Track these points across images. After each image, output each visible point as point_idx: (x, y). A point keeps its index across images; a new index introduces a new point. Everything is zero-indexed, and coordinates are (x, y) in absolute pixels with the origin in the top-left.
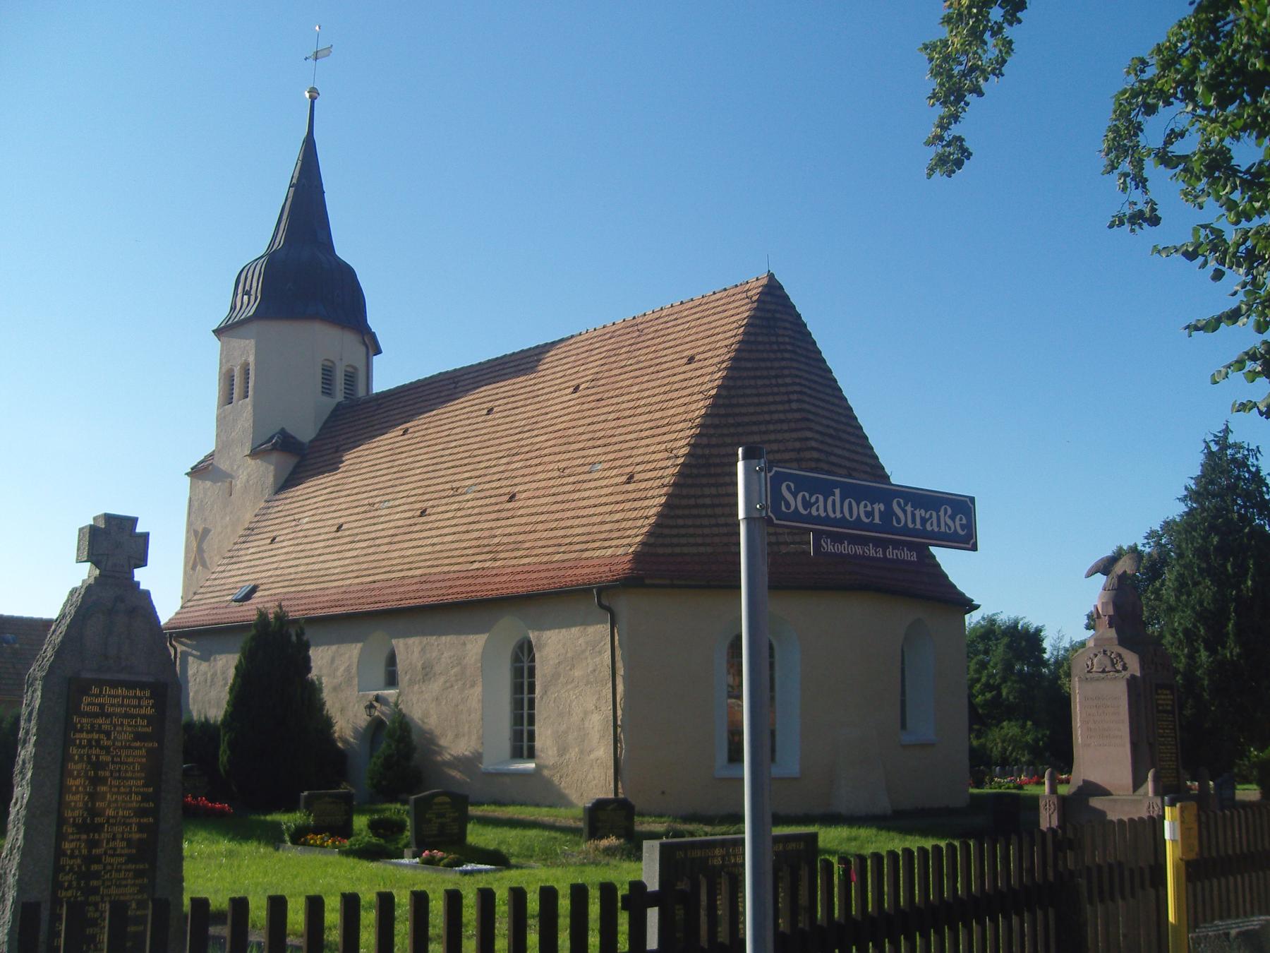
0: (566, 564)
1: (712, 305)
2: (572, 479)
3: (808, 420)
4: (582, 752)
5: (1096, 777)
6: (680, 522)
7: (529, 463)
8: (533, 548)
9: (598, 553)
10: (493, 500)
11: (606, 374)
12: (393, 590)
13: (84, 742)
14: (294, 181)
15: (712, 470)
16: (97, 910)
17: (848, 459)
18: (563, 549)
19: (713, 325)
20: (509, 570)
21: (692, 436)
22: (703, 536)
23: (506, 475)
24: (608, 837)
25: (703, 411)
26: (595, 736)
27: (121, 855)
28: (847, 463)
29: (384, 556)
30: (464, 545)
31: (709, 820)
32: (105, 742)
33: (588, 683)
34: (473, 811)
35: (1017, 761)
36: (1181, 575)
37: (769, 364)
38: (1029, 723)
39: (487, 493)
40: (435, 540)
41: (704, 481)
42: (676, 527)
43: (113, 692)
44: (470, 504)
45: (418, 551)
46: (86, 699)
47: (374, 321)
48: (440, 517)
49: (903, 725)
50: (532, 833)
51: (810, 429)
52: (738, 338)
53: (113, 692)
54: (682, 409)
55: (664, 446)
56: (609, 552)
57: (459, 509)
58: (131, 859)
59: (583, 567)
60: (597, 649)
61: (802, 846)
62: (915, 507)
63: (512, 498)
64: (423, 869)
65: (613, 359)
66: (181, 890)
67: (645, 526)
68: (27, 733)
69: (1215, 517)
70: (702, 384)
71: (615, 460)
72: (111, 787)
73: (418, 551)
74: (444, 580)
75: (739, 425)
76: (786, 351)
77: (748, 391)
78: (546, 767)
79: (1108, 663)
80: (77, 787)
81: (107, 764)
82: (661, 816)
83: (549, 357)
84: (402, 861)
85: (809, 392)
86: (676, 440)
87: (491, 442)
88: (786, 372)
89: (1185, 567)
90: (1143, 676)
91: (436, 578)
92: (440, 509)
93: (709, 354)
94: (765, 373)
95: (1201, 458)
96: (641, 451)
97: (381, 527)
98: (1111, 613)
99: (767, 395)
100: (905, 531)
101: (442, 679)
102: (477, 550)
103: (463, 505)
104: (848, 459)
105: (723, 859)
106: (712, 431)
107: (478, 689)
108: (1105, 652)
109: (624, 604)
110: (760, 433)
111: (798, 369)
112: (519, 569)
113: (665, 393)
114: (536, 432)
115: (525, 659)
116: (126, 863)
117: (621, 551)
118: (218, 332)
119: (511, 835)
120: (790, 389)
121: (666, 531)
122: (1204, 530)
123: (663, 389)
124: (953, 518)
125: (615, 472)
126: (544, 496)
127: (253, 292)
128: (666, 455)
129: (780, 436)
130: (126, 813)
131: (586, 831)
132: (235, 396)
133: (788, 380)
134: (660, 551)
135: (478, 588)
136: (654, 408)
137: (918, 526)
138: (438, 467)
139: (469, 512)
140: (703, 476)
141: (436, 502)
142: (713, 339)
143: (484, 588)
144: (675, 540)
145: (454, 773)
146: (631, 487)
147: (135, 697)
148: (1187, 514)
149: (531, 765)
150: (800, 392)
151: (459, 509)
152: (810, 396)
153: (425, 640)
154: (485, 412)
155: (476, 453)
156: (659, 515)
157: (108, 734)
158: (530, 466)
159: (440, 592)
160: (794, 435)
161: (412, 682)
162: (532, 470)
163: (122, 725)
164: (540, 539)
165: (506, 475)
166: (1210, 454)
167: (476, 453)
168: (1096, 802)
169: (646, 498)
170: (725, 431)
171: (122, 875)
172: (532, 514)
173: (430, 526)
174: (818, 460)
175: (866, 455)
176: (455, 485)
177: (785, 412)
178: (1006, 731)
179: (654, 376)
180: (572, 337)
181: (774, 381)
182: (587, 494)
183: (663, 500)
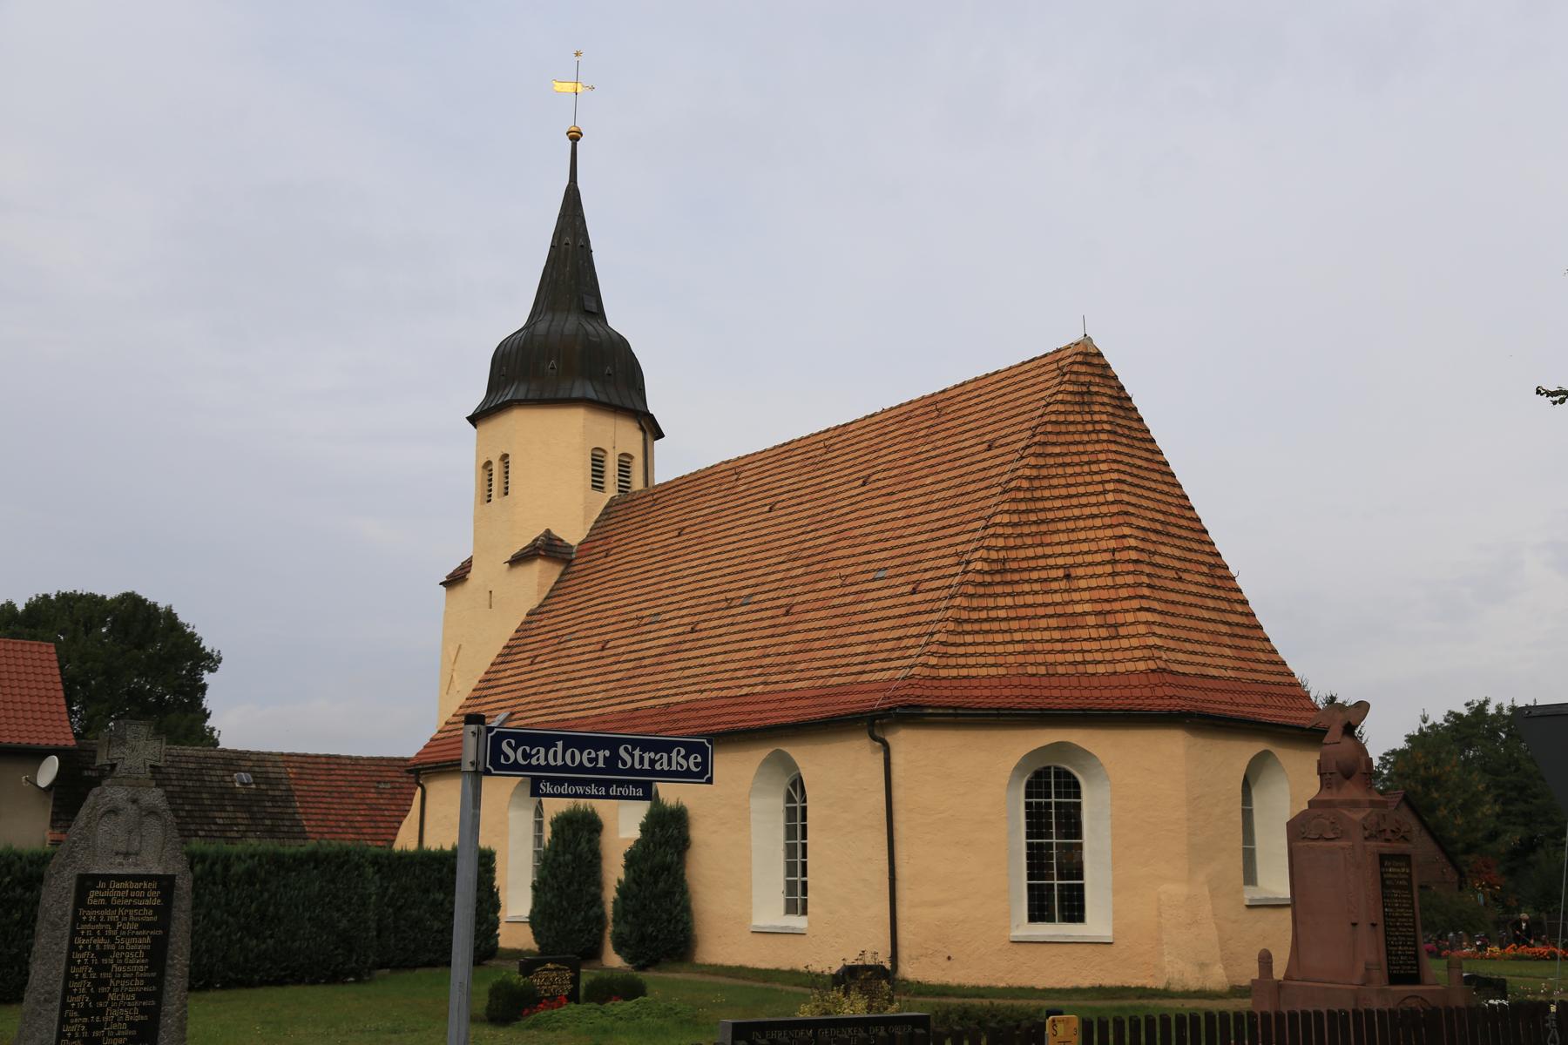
2: (854, 589)
6: (969, 639)
7: (810, 569)
13: (89, 933)
18: (838, 671)
32: (109, 932)
41: (999, 589)
46: (93, 893)
47: (655, 404)
51: (1130, 525)
62: (643, 750)
66: (1363, 1018)
76: (1102, 431)
81: (111, 952)
85: (1129, 479)
94: (1076, 459)
96: (932, 555)
100: (632, 771)
118: (474, 419)
120: (1107, 477)
124: (686, 757)
129: (1091, 535)
132: (494, 493)
133: (1104, 467)
137: (646, 766)
146: (917, 598)
150: (1119, 481)
152: (1131, 484)
157: (113, 924)
160: (1109, 532)
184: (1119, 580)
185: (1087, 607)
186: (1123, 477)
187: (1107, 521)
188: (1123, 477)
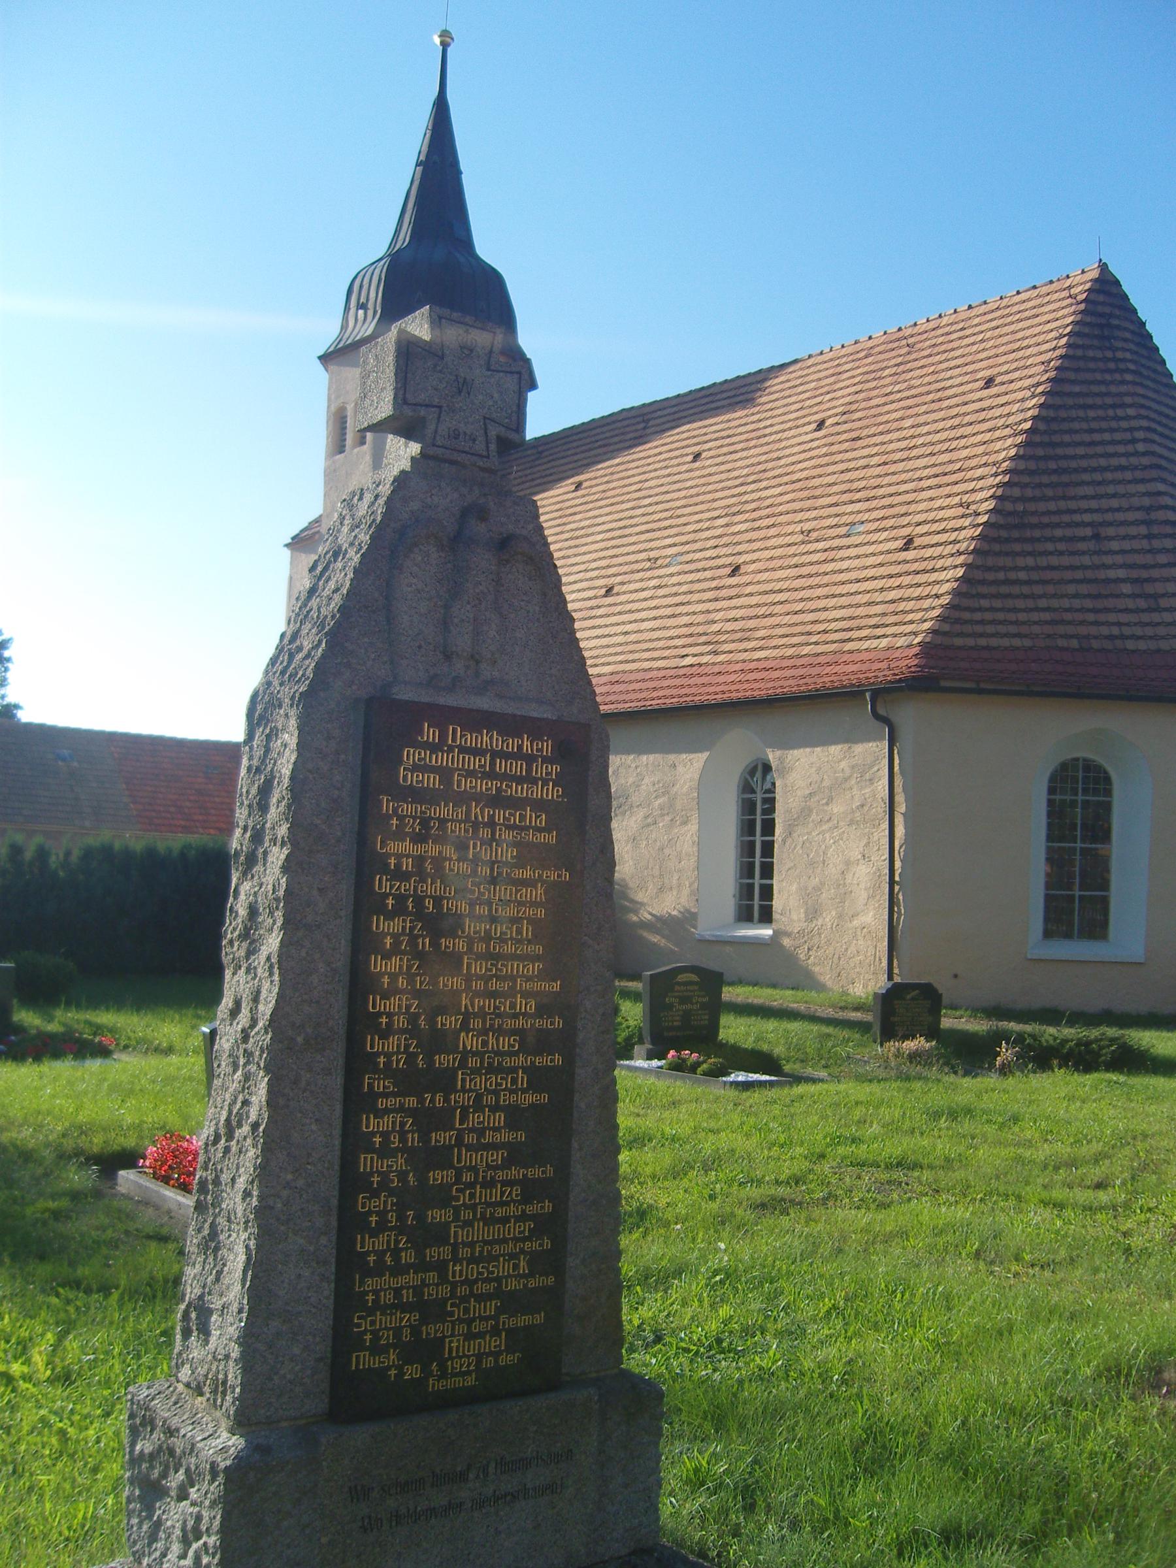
0: (821, 659)
1: (1016, 308)
2: (821, 545)
3: (1159, 467)
4: (840, 916)
6: (985, 603)
7: (757, 524)
8: (771, 637)
9: (866, 644)
10: (708, 574)
11: (863, 405)
14: (422, 158)
15: (1028, 533)
16: (443, 1279)
18: (814, 639)
19: (1020, 335)
20: (738, 667)
21: (997, 486)
22: (1016, 623)
23: (725, 540)
24: (914, 1037)
25: (1013, 452)
26: (861, 895)
27: (494, 1147)
30: (671, 633)
37: (1103, 389)
39: (700, 565)
40: (628, 628)
41: (1017, 547)
43: (471, 740)
44: (675, 580)
45: (604, 641)
46: (410, 755)
48: (634, 596)
50: (795, 1026)
51: (1164, 481)
52: (1058, 352)
53: (471, 740)
54: (981, 450)
55: (957, 500)
56: (884, 642)
57: (660, 587)
58: (515, 1156)
60: (867, 776)
64: (671, 1076)
65: (873, 384)
68: (257, 837)
70: (1009, 415)
71: (883, 518)
72: (468, 979)
73: (604, 641)
74: (644, 680)
75: (1065, 471)
76: (1127, 370)
77: (1076, 425)
78: (788, 935)
80: (393, 977)
83: (775, 384)
84: (632, 1063)
85: (1159, 429)
86: (973, 491)
87: (701, 498)
88: (1128, 400)
91: (633, 677)
93: (1017, 375)
94: (1098, 401)
96: (922, 506)
99: (1101, 431)
101: (641, 813)
102: (690, 640)
106: (1026, 479)
107: (693, 827)
109: (909, 714)
110: (1093, 483)
111: (1144, 396)
112: (753, 665)
113: (953, 428)
114: (764, 484)
116: (508, 1163)
117: (901, 642)
118: (325, 359)
120: (1135, 423)
121: (967, 615)
123: (949, 423)
125: (885, 535)
126: (781, 568)
127: (370, 305)
128: (961, 511)
130: (504, 1043)
131: (877, 1029)
133: (1131, 412)
134: (958, 642)
135: (693, 690)
136: (937, 448)
138: (627, 531)
139: (674, 590)
141: (626, 578)
142: (1020, 354)
144: (979, 629)
145: (655, 939)
146: (910, 555)
147: (519, 755)
149: (766, 932)
150: (1148, 429)
151: (660, 587)
154: (690, 458)
155: (679, 512)
156: (955, 593)
158: (759, 528)
160: (1141, 488)
162: (762, 534)
163: (492, 824)
165: (725, 540)
167: (679, 512)
169: (934, 570)
170: (1045, 479)
171: (495, 1194)
172: (766, 593)
173: (618, 609)
176: (652, 554)
177: (1127, 455)
179: (935, 406)
180: (795, 362)
181: (1111, 412)
182: (845, 565)
183: (960, 572)
184: (1156, 544)
185: (1121, 573)
186: (1154, 425)
187: (1139, 474)
188: (1154, 425)
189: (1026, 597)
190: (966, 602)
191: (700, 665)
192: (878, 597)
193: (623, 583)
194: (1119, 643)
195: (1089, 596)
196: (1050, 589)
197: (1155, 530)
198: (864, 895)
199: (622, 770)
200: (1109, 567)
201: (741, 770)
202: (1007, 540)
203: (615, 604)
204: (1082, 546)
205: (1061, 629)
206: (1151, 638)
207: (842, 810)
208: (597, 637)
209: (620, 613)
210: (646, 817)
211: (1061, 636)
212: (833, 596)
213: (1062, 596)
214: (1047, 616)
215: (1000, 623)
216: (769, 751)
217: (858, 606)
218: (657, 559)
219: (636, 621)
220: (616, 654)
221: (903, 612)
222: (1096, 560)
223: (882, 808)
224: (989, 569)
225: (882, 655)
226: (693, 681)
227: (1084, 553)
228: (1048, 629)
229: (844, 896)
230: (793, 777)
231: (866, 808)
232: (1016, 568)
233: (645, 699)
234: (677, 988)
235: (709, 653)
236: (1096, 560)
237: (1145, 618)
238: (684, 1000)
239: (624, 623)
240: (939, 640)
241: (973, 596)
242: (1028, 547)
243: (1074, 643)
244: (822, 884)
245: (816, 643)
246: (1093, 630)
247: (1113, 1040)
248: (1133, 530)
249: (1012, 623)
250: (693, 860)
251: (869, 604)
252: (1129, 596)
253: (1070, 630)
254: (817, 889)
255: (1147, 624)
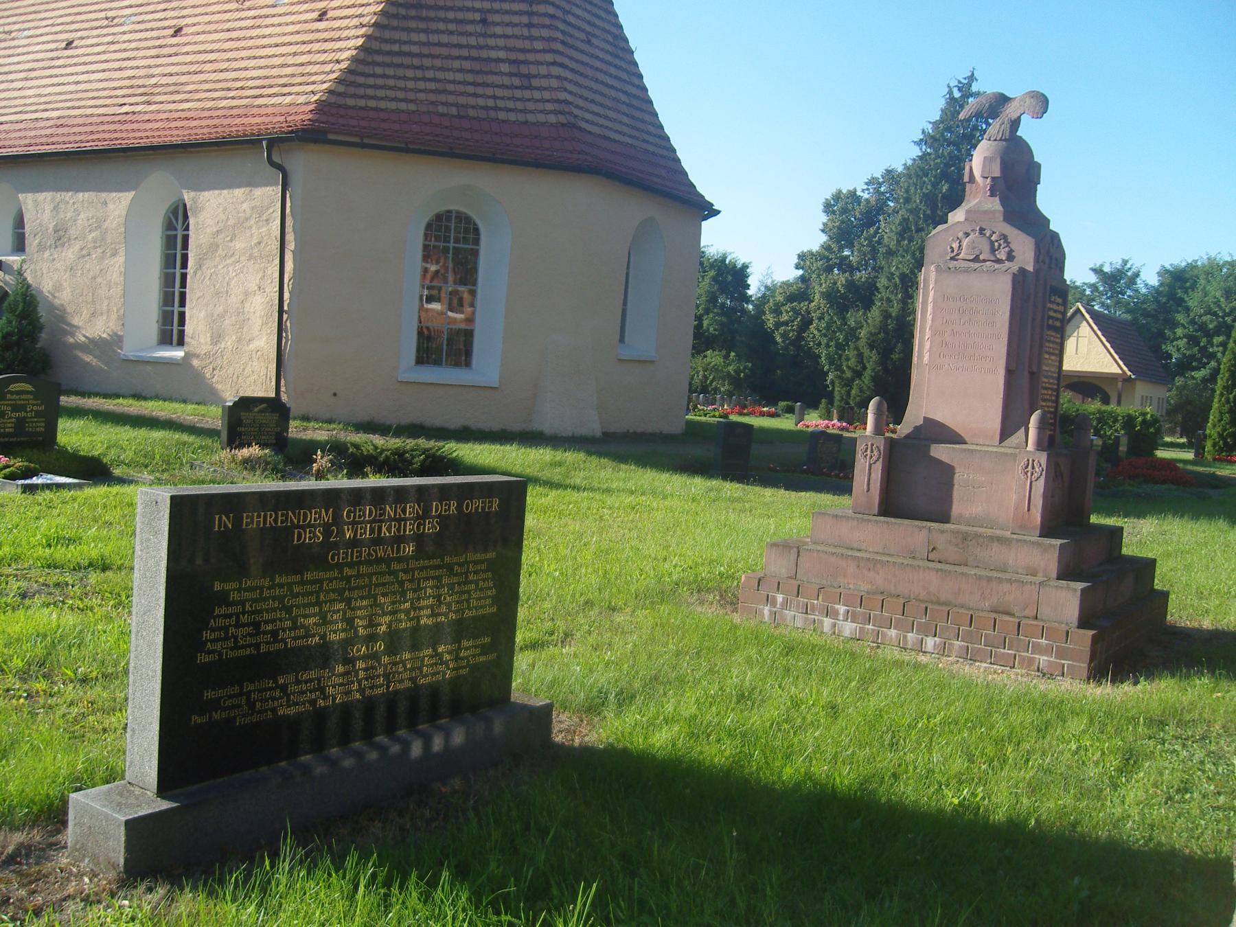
0: (234, 112)
4: (239, 341)
5: (942, 415)
6: (379, 70)
8: (197, 91)
10: (155, 34)
12: (22, 134)
15: (424, 13)
17: (589, 23)
18: (232, 94)
22: (405, 89)
24: (250, 445)
26: (256, 322)
28: (588, 28)
29: (16, 94)
30: (115, 84)
31: (383, 430)
33: (251, 257)
34: (64, 400)
35: (716, 390)
36: (905, 220)
38: (733, 354)
39: (149, 26)
40: (81, 78)
41: (413, 24)
42: (374, 75)
44: (126, 37)
45: (58, 89)
48: (89, 50)
49: (622, 339)
50: (157, 435)
56: (288, 99)
57: (113, 43)
59: (253, 116)
61: (496, 503)
63: (178, 31)
67: (336, 71)
69: (947, 165)
73: (58, 89)
74: (85, 125)
78: (197, 356)
79: (986, 248)
82: (330, 421)
89: (910, 211)
90: (1037, 271)
91: (76, 121)
92: (90, 42)
95: (942, 103)
97: (16, 59)
98: (997, 173)
102: (130, 91)
103: (117, 38)
104: (589, 23)
105: (327, 533)
107: (121, 259)
108: (982, 230)
109: (300, 162)
115: (179, 226)
117: (302, 99)
119: (126, 434)
121: (361, 80)
122: (935, 177)
126: (216, 31)
131: (224, 435)
134: (351, 102)
135: (124, 135)
140: (413, 18)
143: (131, 135)
144: (370, 92)
145: (88, 358)
148: (921, 158)
149: (179, 354)
151: (113, 43)
153: (58, 196)
156: (354, 59)
159: (78, 138)
161: (42, 247)
164: (206, 81)
166: (952, 99)
168: (940, 452)
169: (339, 39)
172: (200, 52)
174: (553, 17)
175: (609, 22)
176: (110, 14)
178: (709, 359)
183: (360, 42)
185: (502, 54)
189: (416, 68)
190: (362, 68)
191: (134, 113)
192: (290, 60)
193: (82, 38)
194: (492, 114)
195: (471, 71)
196: (438, 63)
197: (535, 20)
198: (259, 322)
199: (62, 206)
200: (492, 48)
201: (167, 207)
202: (405, 18)
203: (72, 57)
204: (470, 28)
205: (442, 98)
206: (521, 111)
207: (243, 246)
208: (53, 85)
209: (75, 65)
210: (82, 249)
211: (442, 104)
212: (255, 58)
213: (448, 70)
214: (432, 86)
215: (391, 88)
216: (184, 191)
217: (273, 67)
218: (114, 18)
219: (87, 72)
220: (66, 101)
221: (309, 74)
222: (481, 41)
223: (276, 245)
224: (385, 41)
225: (284, 110)
226: (124, 127)
227: (471, 34)
228: (433, 97)
229: (243, 323)
230: (203, 216)
231: (263, 245)
232: (410, 42)
233: (82, 142)
234: (9, 396)
235: (143, 103)
236: (481, 41)
237: (518, 93)
238: (16, 408)
239: (77, 74)
240: (333, 99)
241: (368, 64)
242: (423, 25)
243: (454, 111)
244: (226, 312)
245: (233, 98)
246: (472, 101)
247: (425, 451)
248: (516, 19)
249: (400, 89)
250: (120, 288)
251: (283, 66)
252: (506, 74)
253: (451, 99)
254: (222, 316)
255: (519, 99)
